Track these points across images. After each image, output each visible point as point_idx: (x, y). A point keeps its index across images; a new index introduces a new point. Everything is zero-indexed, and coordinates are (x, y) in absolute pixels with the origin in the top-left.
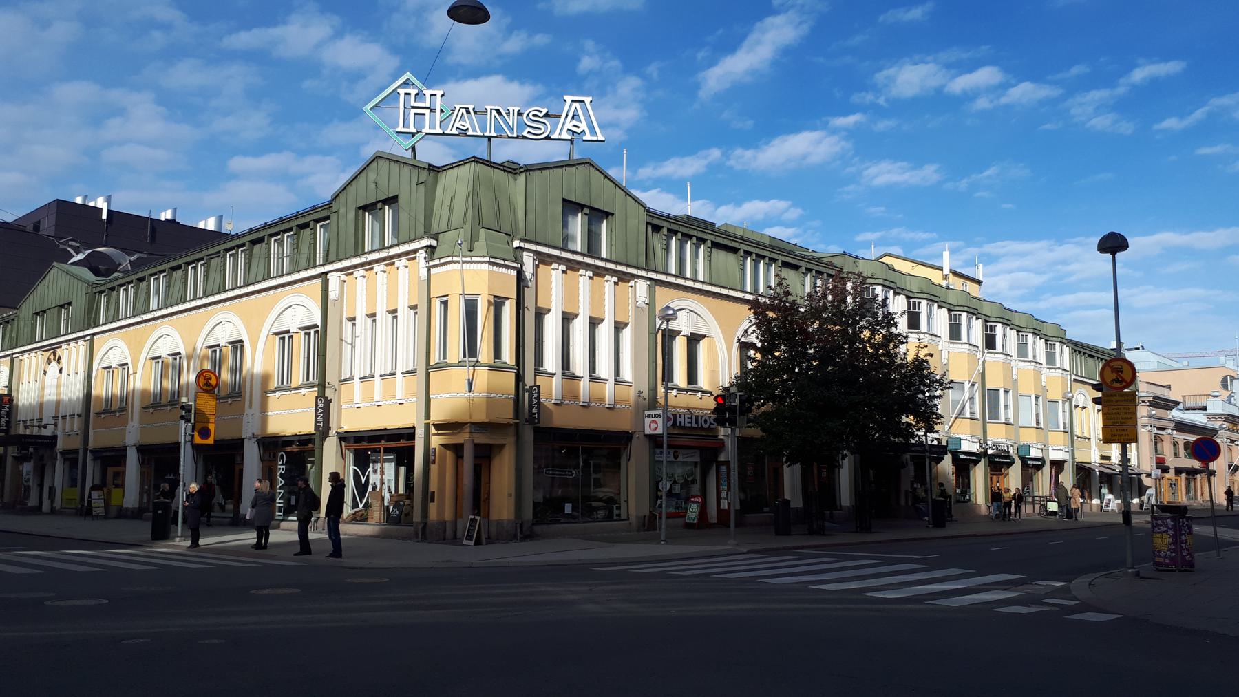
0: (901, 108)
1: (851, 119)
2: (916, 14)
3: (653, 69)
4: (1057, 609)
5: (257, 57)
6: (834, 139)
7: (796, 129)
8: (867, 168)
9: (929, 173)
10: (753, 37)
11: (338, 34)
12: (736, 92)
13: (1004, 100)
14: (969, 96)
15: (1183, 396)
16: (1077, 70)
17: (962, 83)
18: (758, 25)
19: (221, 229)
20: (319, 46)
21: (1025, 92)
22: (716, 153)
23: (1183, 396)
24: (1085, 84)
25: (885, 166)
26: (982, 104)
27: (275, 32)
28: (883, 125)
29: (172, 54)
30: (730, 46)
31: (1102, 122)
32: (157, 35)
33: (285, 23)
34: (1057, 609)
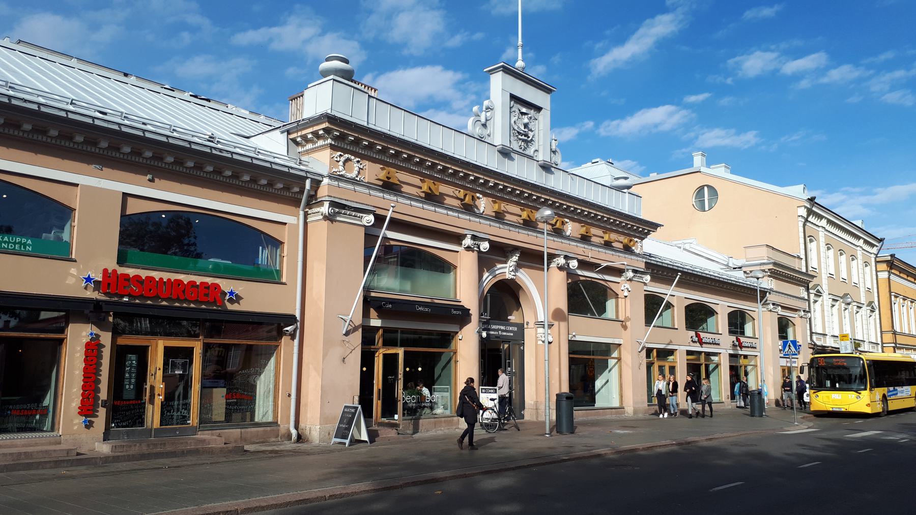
0: (745, 86)
1: (701, 97)
2: (767, 12)
3: (556, 59)
4: (396, 396)
5: (258, 51)
6: (684, 112)
7: (656, 105)
8: (703, 134)
9: (750, 138)
10: (642, 31)
11: (324, 32)
12: (617, 75)
13: (825, 80)
14: (797, 77)
15: (102, 170)
16: (889, 55)
17: (793, 66)
18: (648, 21)
19: (825, 331)
20: (307, 41)
21: (842, 74)
22: (590, 124)
23: (102, 170)
24: (889, 66)
25: (717, 132)
26: (805, 84)
27: (275, 30)
28: (725, 101)
29: (189, 52)
30: (621, 40)
31: (893, 98)
32: (186, 36)
33: (284, 23)
34: (396, 396)
